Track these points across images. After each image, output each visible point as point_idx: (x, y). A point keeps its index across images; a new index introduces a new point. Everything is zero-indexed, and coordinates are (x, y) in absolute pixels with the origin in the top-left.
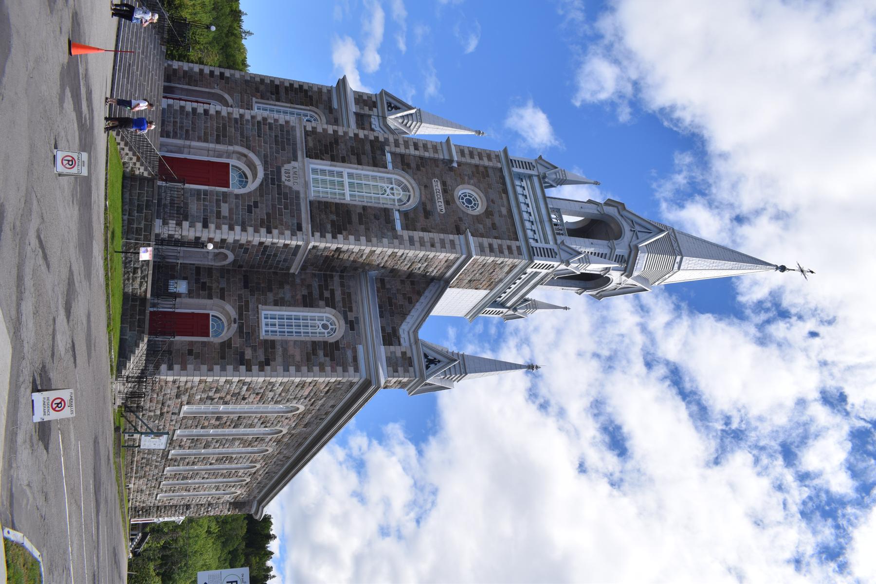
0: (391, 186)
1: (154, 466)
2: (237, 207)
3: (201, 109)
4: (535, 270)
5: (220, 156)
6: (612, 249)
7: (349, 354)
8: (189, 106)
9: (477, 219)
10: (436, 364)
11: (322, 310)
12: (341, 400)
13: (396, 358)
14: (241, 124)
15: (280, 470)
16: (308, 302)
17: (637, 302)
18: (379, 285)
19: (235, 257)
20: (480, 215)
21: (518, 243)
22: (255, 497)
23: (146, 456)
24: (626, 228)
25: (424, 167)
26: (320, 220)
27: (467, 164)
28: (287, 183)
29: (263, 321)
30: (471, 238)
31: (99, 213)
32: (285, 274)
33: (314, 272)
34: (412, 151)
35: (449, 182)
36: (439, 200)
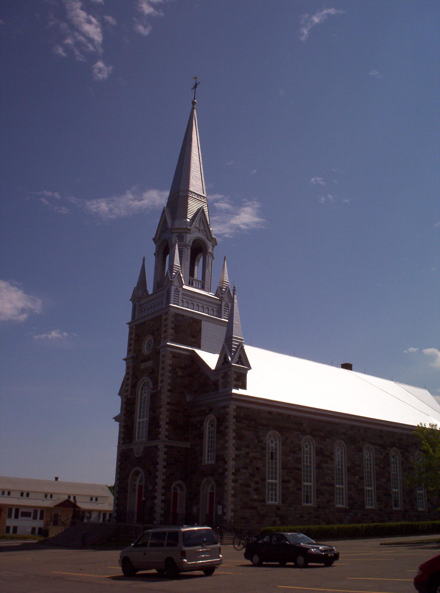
5: (135, 490)
28: (141, 454)
29: (210, 462)
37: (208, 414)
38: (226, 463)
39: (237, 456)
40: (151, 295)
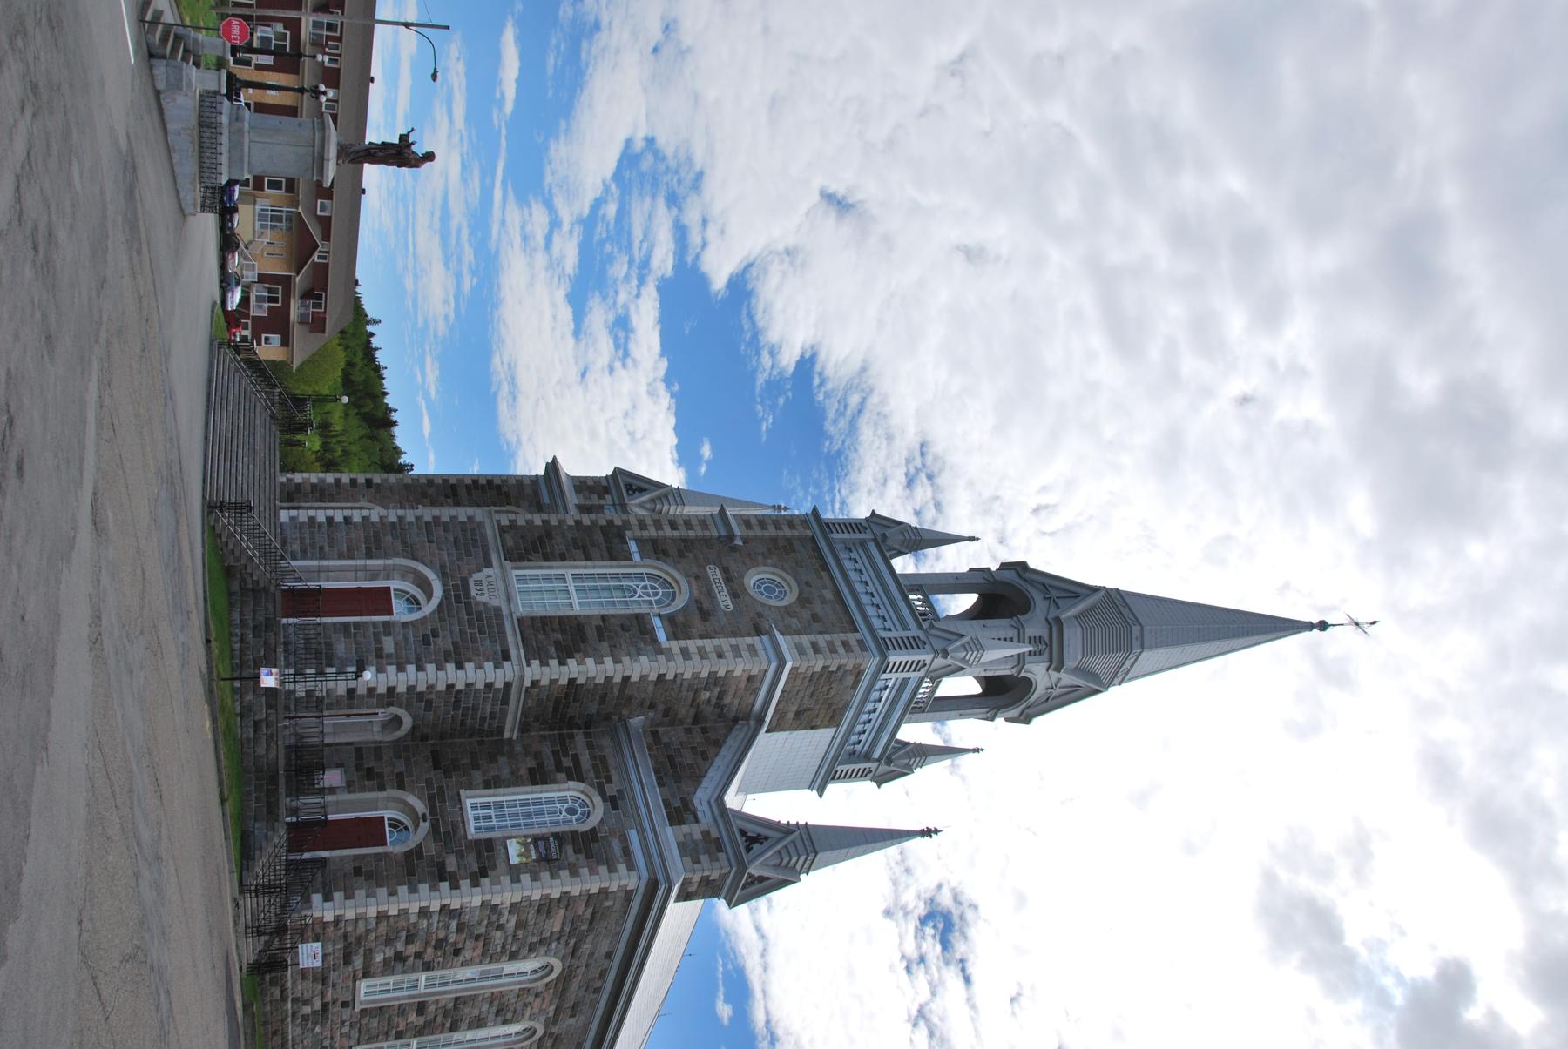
0: (643, 584)
2: (406, 639)
3: (339, 517)
5: (374, 577)
6: (1020, 628)
7: (616, 845)
8: (321, 516)
9: (788, 612)
10: (762, 843)
11: (565, 786)
12: (618, 935)
13: (694, 842)
14: (401, 529)
16: (538, 777)
17: (940, 497)
18: (650, 740)
19: (414, 721)
21: (858, 635)
24: (1037, 597)
25: (690, 552)
26: (537, 644)
28: (479, 598)
29: (470, 814)
30: (780, 638)
33: (542, 733)
34: (668, 532)
35: (733, 566)
36: (721, 593)
37: (602, 793)
38: (475, 883)
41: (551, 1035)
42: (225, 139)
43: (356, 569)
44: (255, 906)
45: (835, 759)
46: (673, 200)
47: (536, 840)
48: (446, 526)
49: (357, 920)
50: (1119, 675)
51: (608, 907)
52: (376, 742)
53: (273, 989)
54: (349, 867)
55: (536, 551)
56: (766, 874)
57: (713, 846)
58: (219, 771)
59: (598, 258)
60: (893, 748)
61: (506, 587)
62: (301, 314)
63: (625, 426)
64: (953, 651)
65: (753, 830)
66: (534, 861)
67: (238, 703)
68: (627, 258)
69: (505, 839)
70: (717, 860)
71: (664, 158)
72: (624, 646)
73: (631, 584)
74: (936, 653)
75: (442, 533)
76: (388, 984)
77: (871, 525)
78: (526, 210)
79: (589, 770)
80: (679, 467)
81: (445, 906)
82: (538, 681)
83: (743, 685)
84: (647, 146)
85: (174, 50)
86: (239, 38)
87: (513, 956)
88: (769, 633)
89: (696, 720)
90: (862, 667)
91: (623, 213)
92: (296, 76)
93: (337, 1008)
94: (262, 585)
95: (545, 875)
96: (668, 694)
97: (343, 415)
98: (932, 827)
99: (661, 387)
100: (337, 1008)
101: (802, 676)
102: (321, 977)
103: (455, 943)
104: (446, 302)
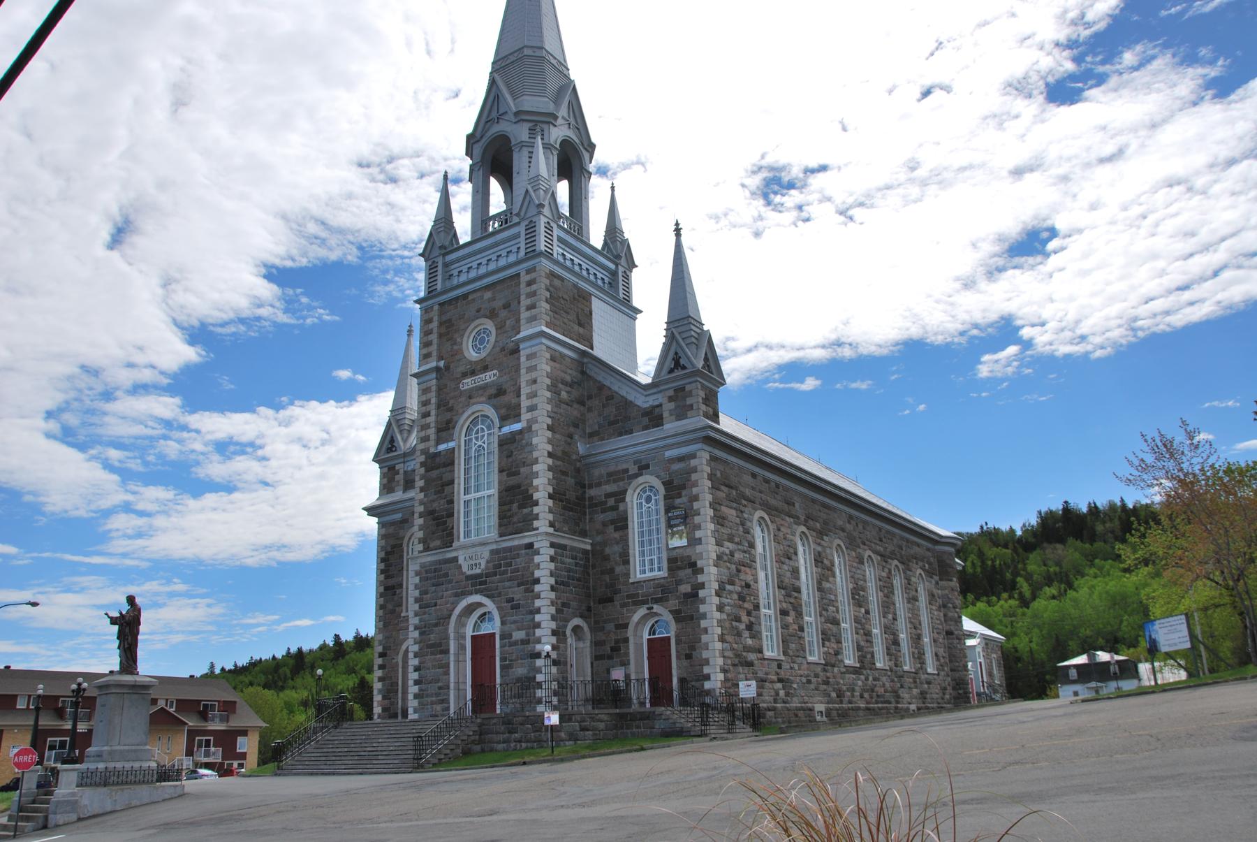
0: (474, 440)
1: (875, 683)
2: (515, 622)
3: (413, 676)
4: (555, 242)
5: (463, 647)
6: (522, 145)
7: (676, 467)
10: (680, 357)
12: (740, 468)
13: (676, 408)
15: (874, 525)
16: (621, 524)
18: (596, 438)
19: (576, 616)
20: (496, 325)
22: (928, 550)
23: (857, 694)
24: (495, 129)
27: (439, 350)
28: (483, 566)
29: (649, 575)
30: (522, 334)
31: (454, 776)
32: (593, 555)
34: (431, 419)
35: (461, 369)
38: (698, 571)
39: (719, 557)
40: (467, 244)
41: (806, 521)
42: (119, 765)
43: (457, 661)
44: (714, 727)
45: (616, 298)
46: (108, 395)
47: (670, 526)
48: (423, 593)
49: (724, 657)
50: (561, 69)
51: (721, 474)
52: (591, 647)
53: (768, 717)
54: (685, 663)
55: (445, 523)
56: (703, 355)
57: (680, 395)
58: (621, 752)
59: (159, 467)
60: (608, 252)
61: (474, 545)
62: (221, 720)
63: (316, 448)
64: (538, 199)
65: (669, 363)
66: (686, 527)
67: (567, 743)
68: (162, 442)
69: (669, 549)
70: (691, 391)
71: (67, 402)
72: (524, 455)
73: (474, 449)
74: (539, 213)
75: (428, 596)
76: (767, 636)
77: (431, 257)
78: (114, 534)
79: (618, 486)
80: (356, 401)
81: (716, 593)
82: (550, 522)
83: (558, 366)
84: (54, 418)
85: (36, 810)
86: (30, 756)
87: (752, 545)
88: (517, 343)
89: (582, 403)
90: (548, 272)
91: (118, 444)
92: (5, 732)
93: (782, 672)
94: (476, 729)
95: (697, 519)
96: (562, 424)
97: (294, 691)
98: (674, 227)
99: (283, 414)
100: (782, 672)
101: (553, 319)
102: (761, 682)
103: (742, 587)
104: (195, 606)
